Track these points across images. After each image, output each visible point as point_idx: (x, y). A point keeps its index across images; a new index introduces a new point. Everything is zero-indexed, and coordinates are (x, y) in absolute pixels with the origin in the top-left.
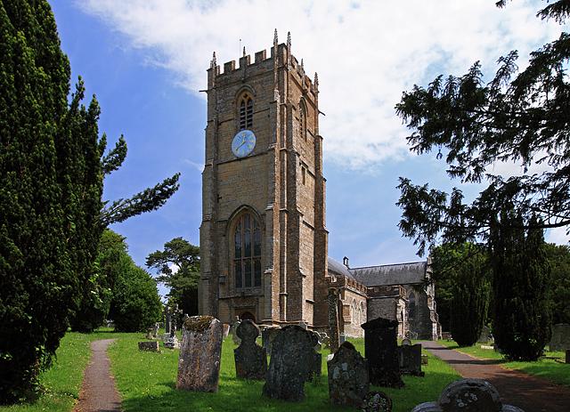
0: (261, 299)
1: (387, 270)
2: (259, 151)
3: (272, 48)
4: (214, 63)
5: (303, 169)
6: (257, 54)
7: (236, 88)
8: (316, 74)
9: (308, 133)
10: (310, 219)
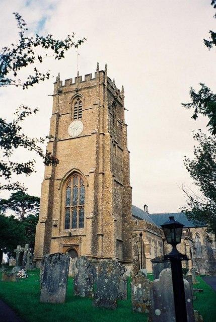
4: (58, 79)
5: (114, 145)
7: (72, 94)
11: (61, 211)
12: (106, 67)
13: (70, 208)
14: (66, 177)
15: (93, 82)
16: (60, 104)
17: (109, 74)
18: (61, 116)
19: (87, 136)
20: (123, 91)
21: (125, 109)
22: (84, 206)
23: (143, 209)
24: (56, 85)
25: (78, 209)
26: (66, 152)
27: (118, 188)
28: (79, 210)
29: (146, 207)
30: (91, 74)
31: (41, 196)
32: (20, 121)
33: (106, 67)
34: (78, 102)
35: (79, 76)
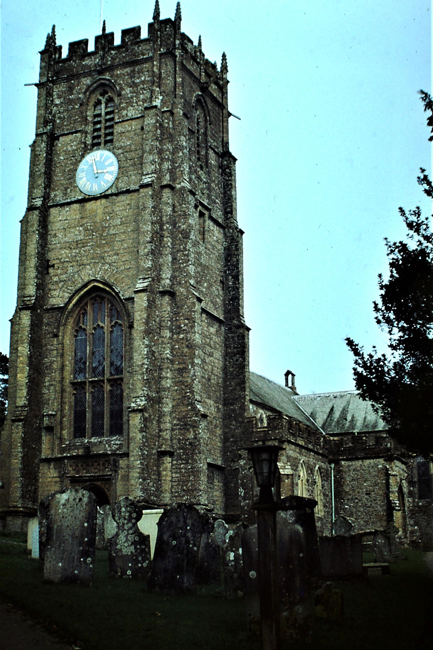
0: (122, 463)
1: (246, 350)
2: (123, 186)
3: (150, 26)
4: (51, 39)
5: (201, 215)
6: (125, 33)
7: (87, 81)
8: (224, 56)
9: (211, 152)
10: (214, 304)
11: (63, 391)
12: (200, 40)
13: (85, 383)
14: (74, 302)
15: (143, 47)
16: (56, 105)
17: (184, 28)
18: (57, 138)
19: (128, 192)
20: (225, 68)
21: (230, 114)
22: (122, 379)
23: (282, 382)
24: (46, 55)
25: (107, 387)
26: (71, 237)
27: (213, 330)
28: (109, 388)
29: (290, 376)
30: (139, 28)
31: (11, 353)
32: (338, 397)
33: (200, 40)
34: (103, 100)
35: (107, 32)
